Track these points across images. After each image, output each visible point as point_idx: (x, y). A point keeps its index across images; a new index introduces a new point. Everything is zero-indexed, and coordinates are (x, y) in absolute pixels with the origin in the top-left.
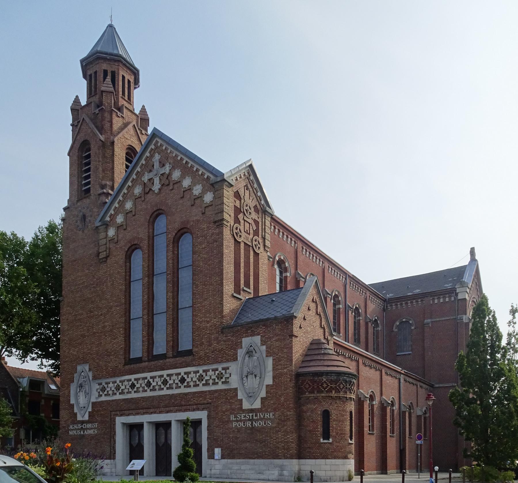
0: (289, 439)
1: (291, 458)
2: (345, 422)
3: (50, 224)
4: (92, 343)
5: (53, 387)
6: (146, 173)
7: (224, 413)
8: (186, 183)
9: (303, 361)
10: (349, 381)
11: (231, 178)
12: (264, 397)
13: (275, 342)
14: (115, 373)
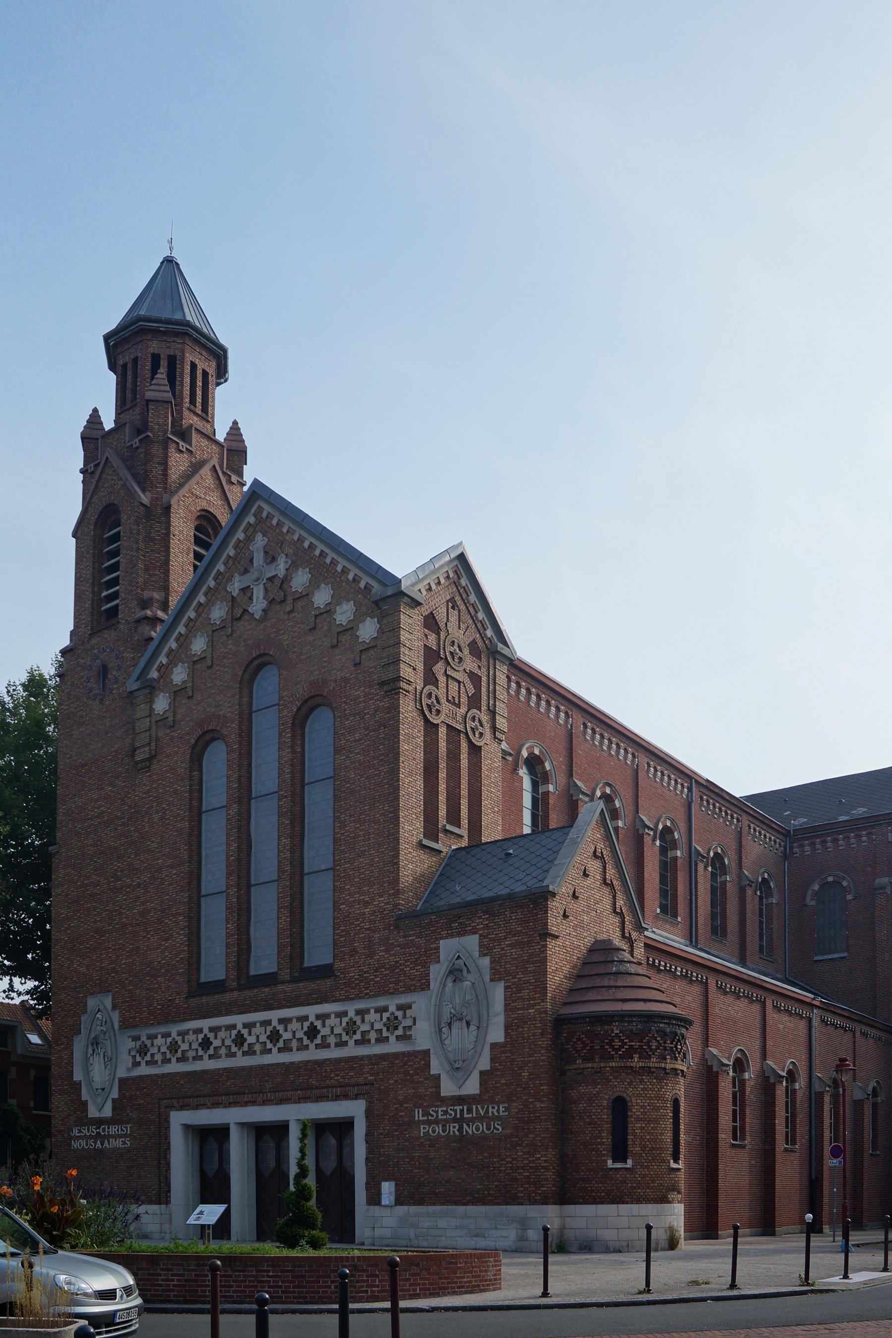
0: (540, 1161)
1: (545, 1202)
2: (661, 1123)
3: (33, 675)
4: (119, 949)
5: (35, 1039)
6: (237, 577)
7: (401, 1106)
8: (322, 597)
9: (571, 990)
10: (671, 1032)
11: (416, 588)
12: (486, 1071)
13: (510, 948)
14: (169, 1015)
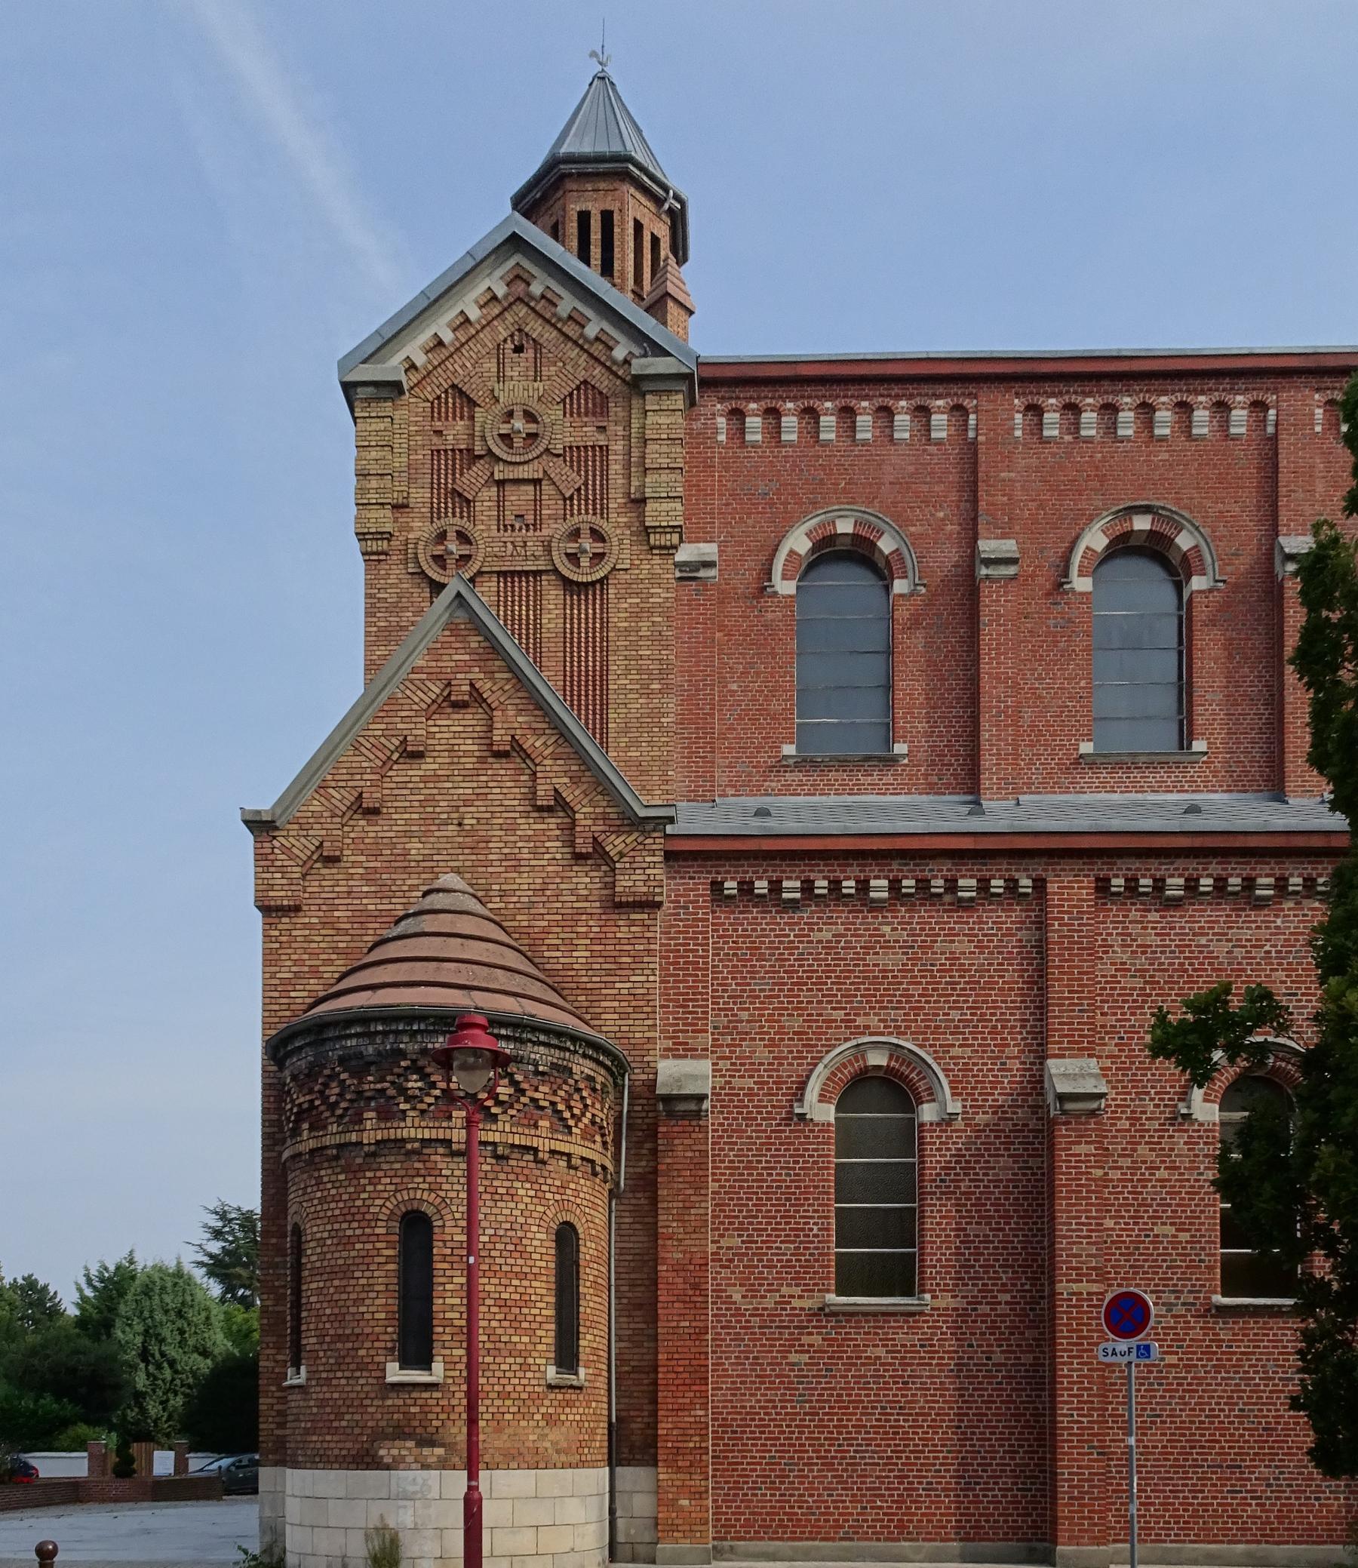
2: (357, 1274)
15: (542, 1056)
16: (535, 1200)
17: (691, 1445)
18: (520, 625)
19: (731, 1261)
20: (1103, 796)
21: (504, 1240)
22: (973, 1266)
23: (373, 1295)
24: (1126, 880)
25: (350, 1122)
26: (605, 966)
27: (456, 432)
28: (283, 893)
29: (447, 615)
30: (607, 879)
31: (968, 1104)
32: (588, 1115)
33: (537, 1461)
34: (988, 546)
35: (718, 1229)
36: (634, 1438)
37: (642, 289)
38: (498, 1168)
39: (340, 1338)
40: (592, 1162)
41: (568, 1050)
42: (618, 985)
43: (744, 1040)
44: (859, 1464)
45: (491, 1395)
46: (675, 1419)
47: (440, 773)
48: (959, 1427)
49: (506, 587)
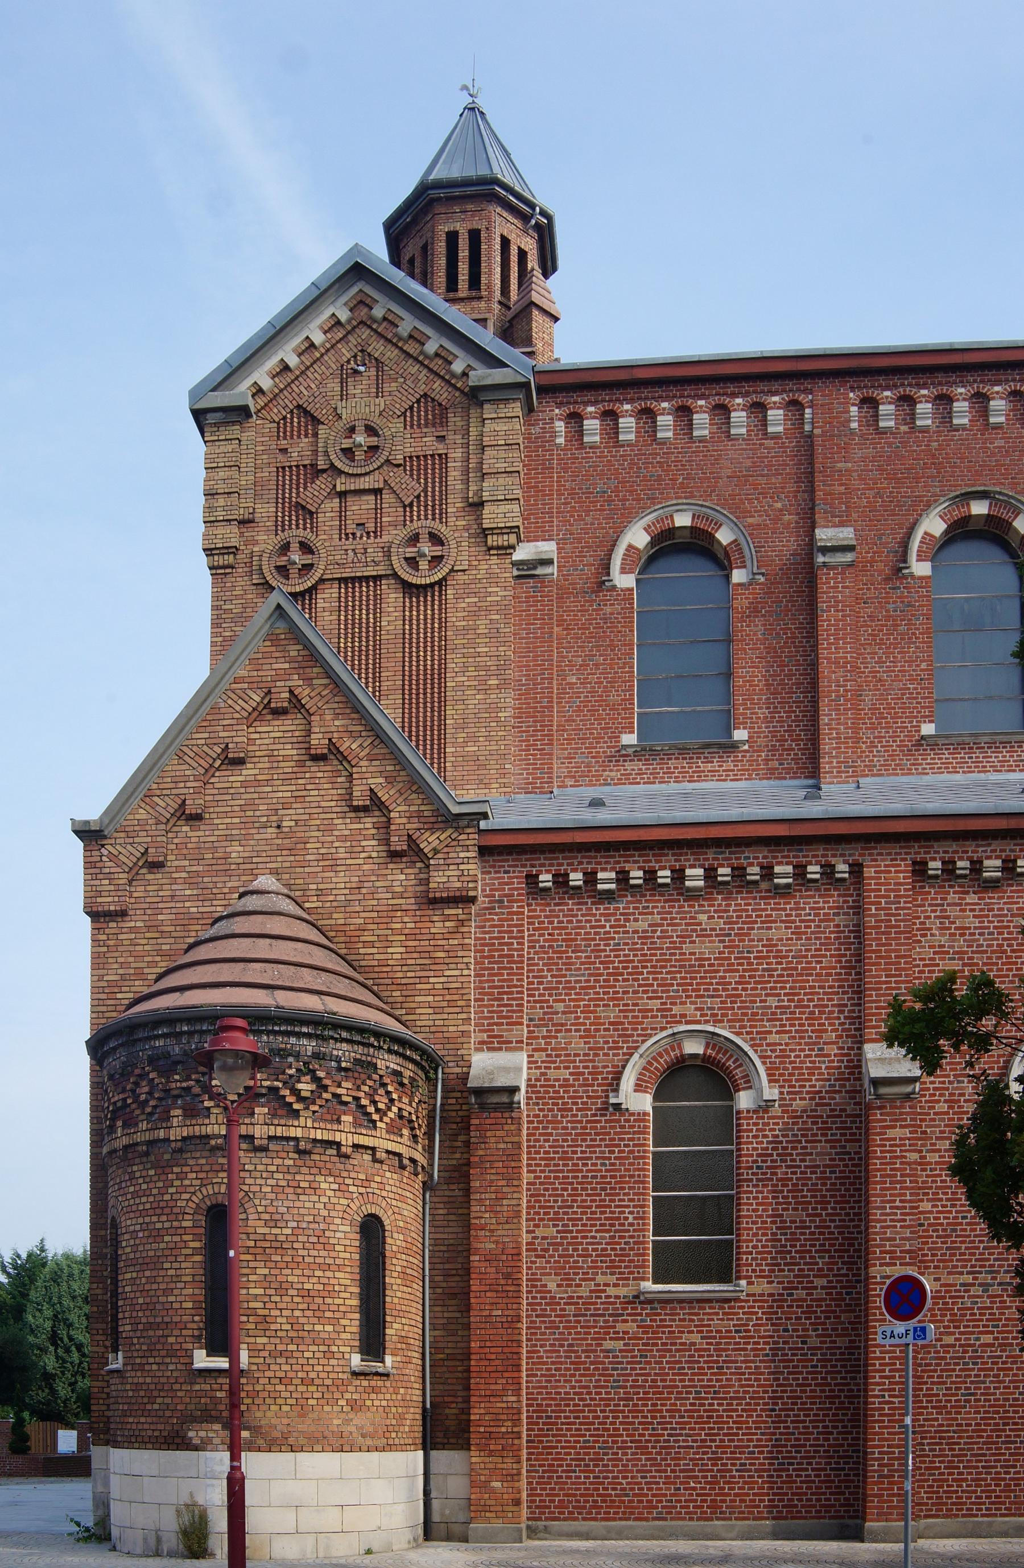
2: (167, 1265)
15: (344, 1052)
16: (338, 1194)
17: (503, 1429)
18: (360, 628)
19: (546, 1250)
20: (945, 776)
21: (306, 1232)
22: (790, 1252)
23: (180, 1285)
24: (943, 863)
25: (159, 1119)
26: (419, 961)
27: (300, 450)
28: (110, 899)
29: (268, 626)
30: (422, 876)
31: (785, 1090)
32: (395, 1109)
33: (342, 1445)
34: (824, 535)
35: (534, 1219)
36: (448, 1423)
37: (509, 299)
38: (300, 1163)
39: (150, 1326)
40: (399, 1155)
41: (373, 1046)
42: (432, 980)
43: (560, 1031)
44: (673, 1447)
45: (294, 1382)
46: (488, 1405)
47: (260, 777)
48: (774, 1410)
49: (346, 593)
